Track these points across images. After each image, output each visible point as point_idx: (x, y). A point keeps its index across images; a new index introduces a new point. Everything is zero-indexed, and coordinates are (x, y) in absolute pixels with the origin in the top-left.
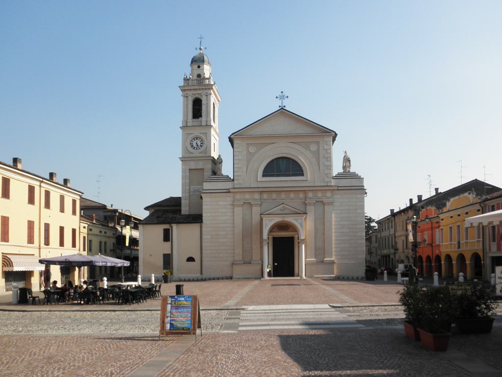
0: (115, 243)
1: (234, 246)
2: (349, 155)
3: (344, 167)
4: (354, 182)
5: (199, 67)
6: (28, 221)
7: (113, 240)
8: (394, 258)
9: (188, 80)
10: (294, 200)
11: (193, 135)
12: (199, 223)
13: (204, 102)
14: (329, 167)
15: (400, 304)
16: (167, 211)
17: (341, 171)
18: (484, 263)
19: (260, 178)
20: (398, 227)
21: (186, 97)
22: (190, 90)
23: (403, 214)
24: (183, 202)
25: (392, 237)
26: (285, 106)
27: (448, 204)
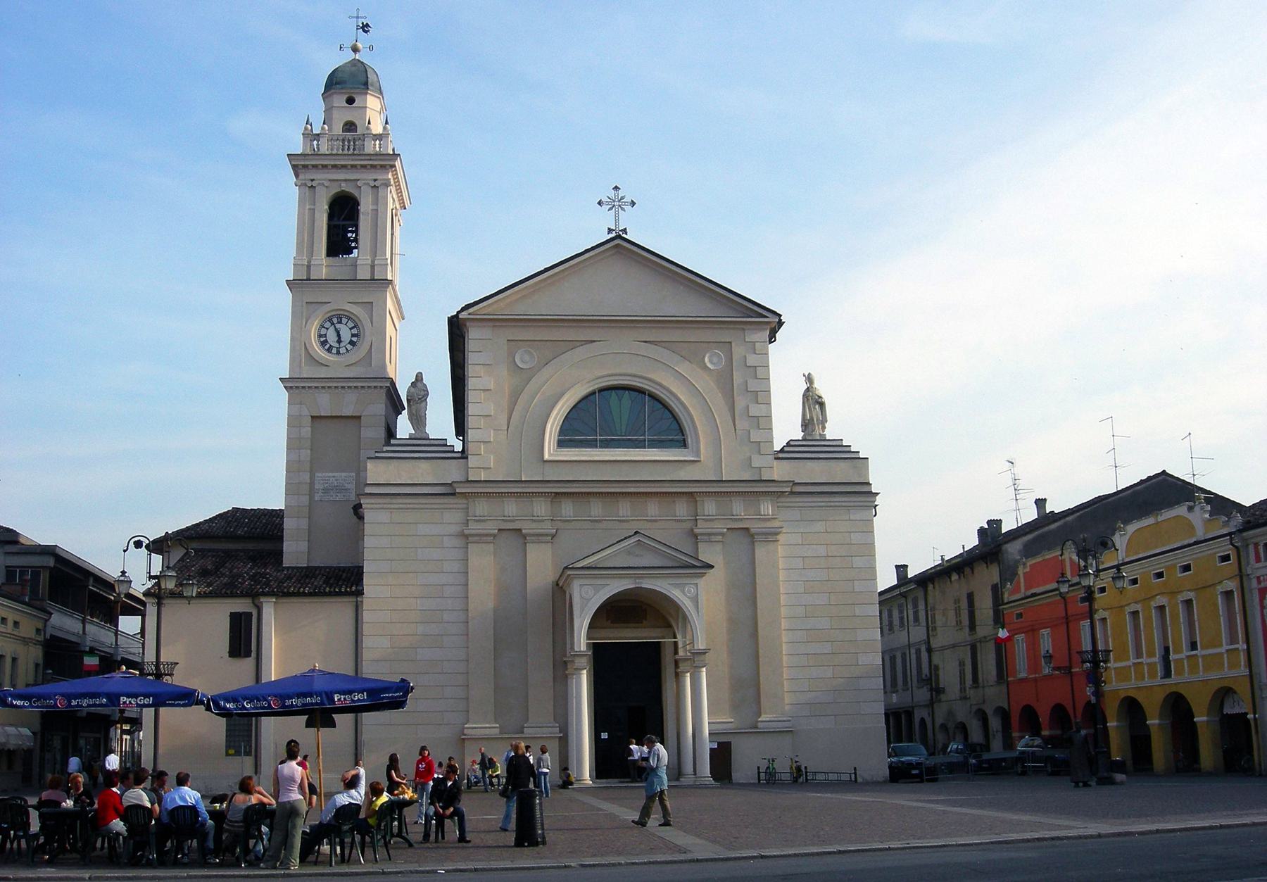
0: (41, 661)
1: (468, 673)
2: (821, 388)
3: (807, 425)
4: (839, 472)
5: (350, 101)
6: (335, 726)
7: (36, 653)
8: (928, 721)
9: (317, 137)
10: (604, 525)
11: (327, 308)
12: (346, 594)
13: (365, 206)
14: (763, 422)
15: (48, 637)
16: (229, 555)
17: (799, 435)
18: (1255, 719)
19: (550, 450)
20: (940, 619)
21: (308, 189)
22: (324, 167)
23: (955, 577)
24: (288, 524)
25: (918, 652)
26: (625, 231)
27: (1120, 540)
